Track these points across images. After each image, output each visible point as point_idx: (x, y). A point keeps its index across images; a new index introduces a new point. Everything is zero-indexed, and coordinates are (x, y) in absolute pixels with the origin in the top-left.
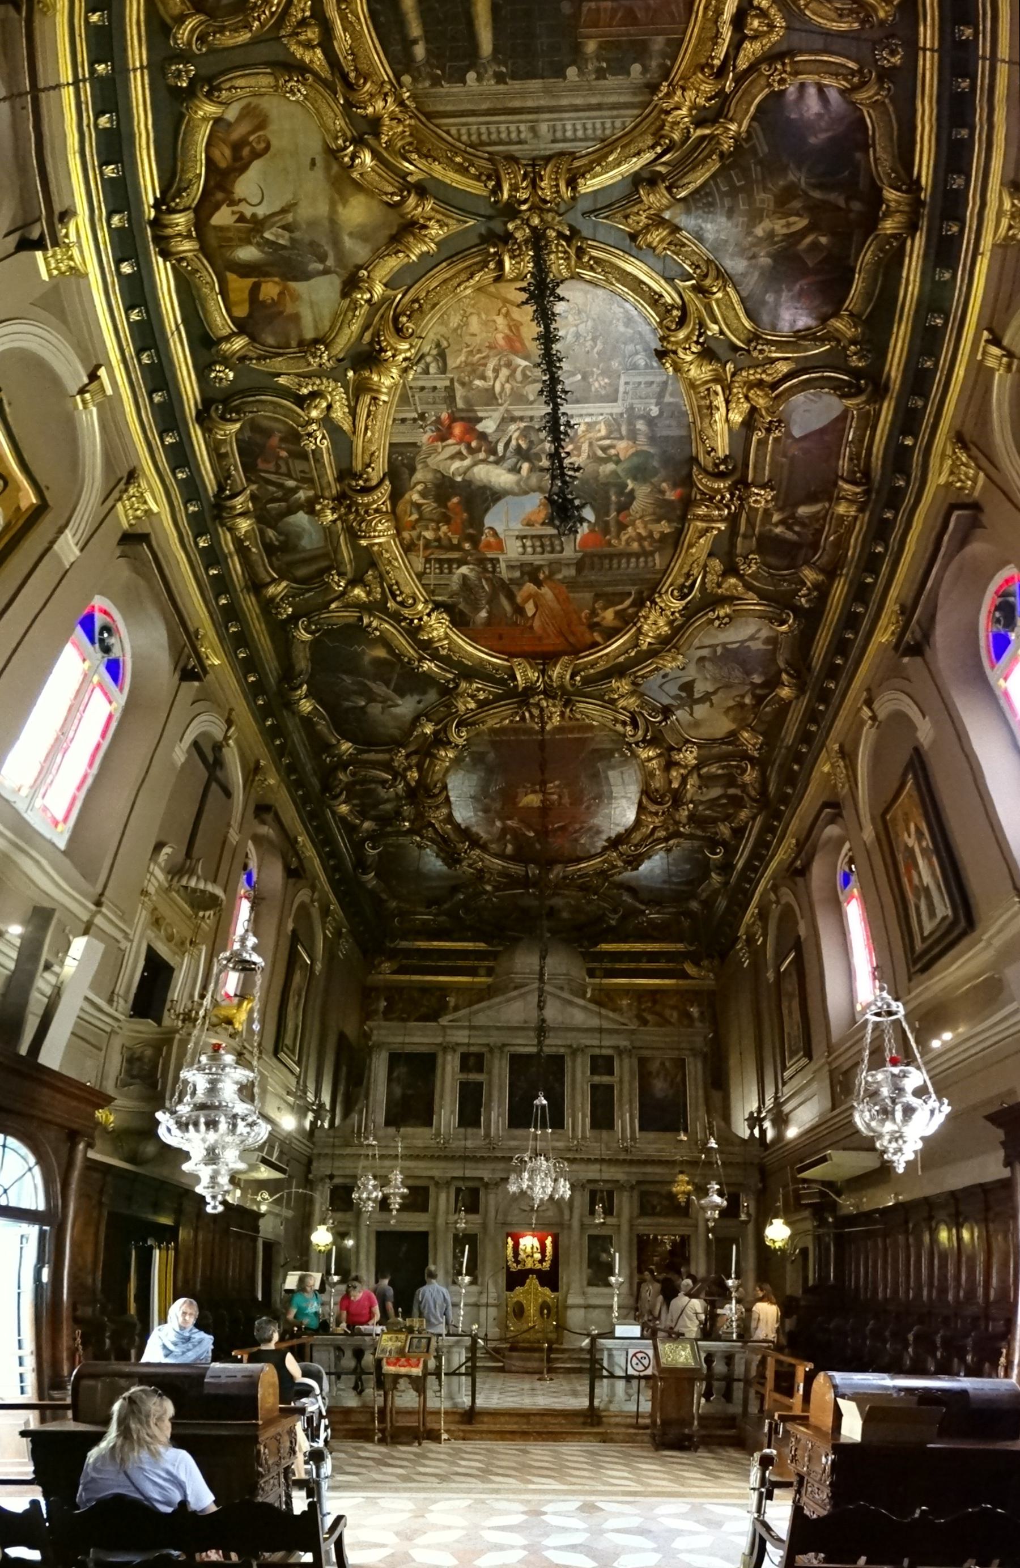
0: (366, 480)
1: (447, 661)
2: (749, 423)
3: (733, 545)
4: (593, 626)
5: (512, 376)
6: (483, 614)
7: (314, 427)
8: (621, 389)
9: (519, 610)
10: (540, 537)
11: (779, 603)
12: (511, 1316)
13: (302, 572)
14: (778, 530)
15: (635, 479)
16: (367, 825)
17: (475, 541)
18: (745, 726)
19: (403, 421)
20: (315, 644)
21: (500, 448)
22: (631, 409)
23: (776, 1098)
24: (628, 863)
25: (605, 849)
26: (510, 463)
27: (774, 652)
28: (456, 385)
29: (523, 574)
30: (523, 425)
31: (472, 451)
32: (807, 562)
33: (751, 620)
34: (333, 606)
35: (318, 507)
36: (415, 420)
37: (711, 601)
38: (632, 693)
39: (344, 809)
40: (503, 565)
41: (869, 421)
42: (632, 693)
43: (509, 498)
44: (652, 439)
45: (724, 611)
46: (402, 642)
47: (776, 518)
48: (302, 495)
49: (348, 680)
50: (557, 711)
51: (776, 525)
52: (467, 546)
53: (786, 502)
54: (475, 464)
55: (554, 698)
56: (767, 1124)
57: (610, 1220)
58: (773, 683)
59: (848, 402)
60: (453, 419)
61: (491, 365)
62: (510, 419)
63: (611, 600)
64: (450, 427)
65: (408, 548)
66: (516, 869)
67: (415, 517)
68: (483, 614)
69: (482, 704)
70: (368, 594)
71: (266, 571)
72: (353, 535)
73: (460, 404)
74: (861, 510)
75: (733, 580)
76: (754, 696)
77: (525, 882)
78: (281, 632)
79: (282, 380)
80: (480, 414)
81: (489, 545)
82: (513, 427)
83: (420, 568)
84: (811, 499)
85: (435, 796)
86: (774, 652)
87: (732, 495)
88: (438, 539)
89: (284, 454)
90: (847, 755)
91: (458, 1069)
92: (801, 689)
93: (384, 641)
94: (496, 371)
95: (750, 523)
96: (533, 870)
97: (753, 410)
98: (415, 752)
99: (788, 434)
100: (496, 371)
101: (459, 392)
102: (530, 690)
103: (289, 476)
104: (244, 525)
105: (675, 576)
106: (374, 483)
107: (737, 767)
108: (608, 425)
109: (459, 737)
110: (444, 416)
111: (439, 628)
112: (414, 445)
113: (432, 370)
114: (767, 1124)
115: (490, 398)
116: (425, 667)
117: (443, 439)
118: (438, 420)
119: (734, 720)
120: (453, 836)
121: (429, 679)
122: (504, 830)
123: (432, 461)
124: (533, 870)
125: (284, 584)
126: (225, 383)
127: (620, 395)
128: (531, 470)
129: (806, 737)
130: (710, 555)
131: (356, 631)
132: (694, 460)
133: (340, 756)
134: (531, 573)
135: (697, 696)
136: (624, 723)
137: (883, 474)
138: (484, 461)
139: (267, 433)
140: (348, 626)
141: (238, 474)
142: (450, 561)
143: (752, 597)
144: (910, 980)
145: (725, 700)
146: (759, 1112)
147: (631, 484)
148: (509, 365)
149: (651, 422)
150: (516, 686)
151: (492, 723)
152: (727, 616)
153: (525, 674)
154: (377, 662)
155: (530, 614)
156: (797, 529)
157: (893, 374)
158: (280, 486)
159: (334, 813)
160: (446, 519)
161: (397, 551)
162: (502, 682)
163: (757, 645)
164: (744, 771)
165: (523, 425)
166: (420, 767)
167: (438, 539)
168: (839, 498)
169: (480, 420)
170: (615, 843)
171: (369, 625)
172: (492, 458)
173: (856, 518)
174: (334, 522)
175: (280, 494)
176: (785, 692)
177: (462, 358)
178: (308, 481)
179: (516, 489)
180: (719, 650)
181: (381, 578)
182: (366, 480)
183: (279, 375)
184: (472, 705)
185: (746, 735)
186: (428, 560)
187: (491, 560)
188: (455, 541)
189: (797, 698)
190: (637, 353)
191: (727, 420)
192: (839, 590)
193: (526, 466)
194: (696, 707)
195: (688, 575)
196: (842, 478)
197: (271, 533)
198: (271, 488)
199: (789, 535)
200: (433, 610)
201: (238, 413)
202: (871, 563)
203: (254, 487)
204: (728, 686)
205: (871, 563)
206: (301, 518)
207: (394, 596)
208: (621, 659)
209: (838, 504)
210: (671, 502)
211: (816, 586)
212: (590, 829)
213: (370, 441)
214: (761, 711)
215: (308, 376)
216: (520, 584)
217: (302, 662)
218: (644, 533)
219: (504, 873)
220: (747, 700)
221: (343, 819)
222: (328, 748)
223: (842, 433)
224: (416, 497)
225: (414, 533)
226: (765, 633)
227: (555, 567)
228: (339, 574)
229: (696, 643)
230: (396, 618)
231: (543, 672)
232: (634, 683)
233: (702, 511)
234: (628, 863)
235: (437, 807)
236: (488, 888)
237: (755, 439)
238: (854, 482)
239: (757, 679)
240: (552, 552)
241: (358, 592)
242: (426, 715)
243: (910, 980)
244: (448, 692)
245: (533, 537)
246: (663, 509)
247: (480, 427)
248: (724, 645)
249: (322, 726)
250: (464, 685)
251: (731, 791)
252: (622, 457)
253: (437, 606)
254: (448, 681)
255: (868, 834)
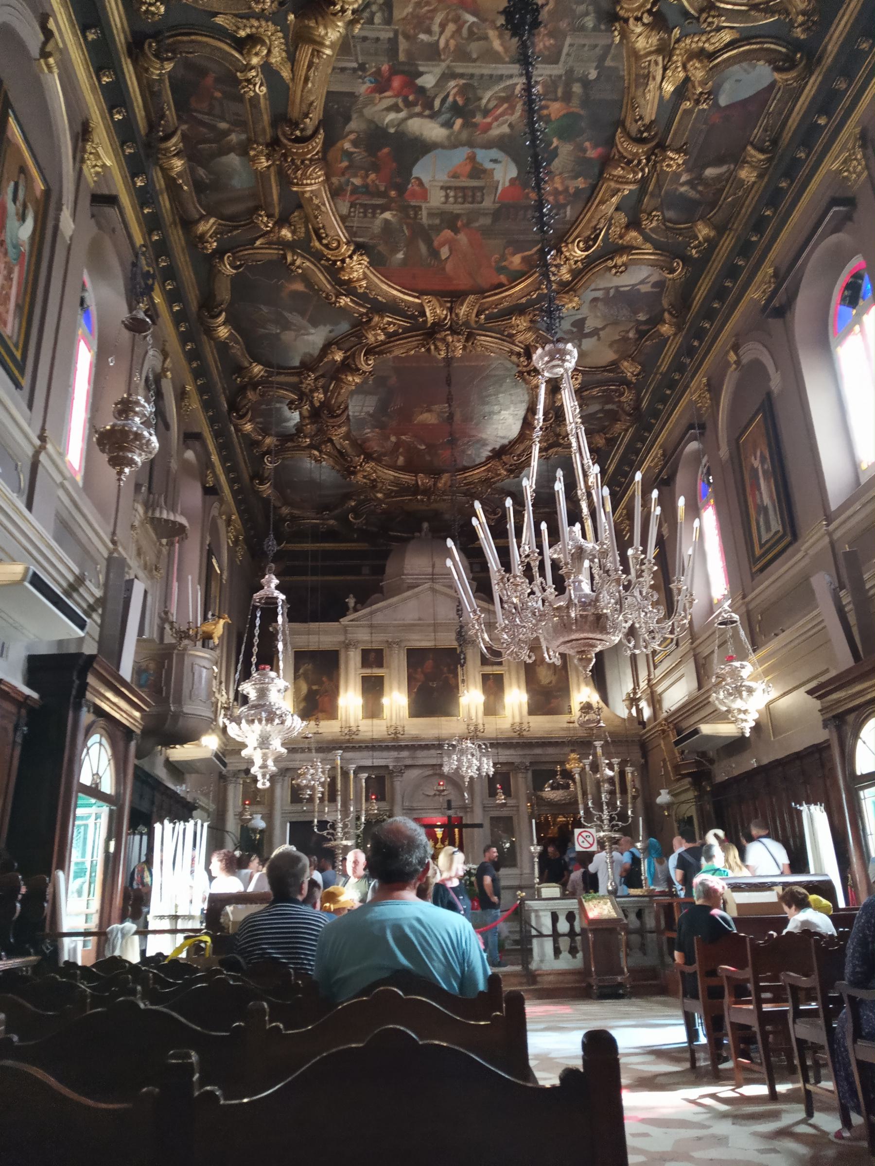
0: (302, 130)
1: (363, 298)
2: (682, 91)
3: (640, 201)
4: (501, 270)
5: (458, 31)
6: (400, 255)
7: (253, 73)
8: (565, 50)
9: (434, 253)
10: (463, 189)
11: (670, 252)
12: (576, 912)
13: (231, 210)
14: (683, 189)
15: (560, 138)
16: (268, 440)
17: (401, 189)
18: (625, 356)
19: (343, 70)
20: (235, 280)
21: (437, 103)
22: (570, 72)
23: (649, 680)
24: (511, 471)
25: (489, 458)
26: (445, 117)
27: (659, 295)
28: (401, 39)
29: (442, 221)
30: (462, 82)
31: (409, 104)
32: (702, 218)
33: (643, 267)
34: (258, 243)
35: (252, 153)
36: (354, 70)
37: (612, 250)
38: (529, 329)
39: (248, 427)
40: (424, 213)
41: (794, 95)
42: (529, 329)
43: (438, 151)
44: (586, 102)
45: (619, 260)
46: (322, 279)
47: (684, 178)
48: (233, 138)
49: (265, 309)
50: (460, 345)
51: (683, 184)
52: (393, 193)
53: (696, 166)
54: (411, 116)
55: (459, 334)
56: (643, 704)
57: (511, 802)
58: (656, 320)
59: (777, 76)
60: (394, 72)
61: (438, 19)
62: (445, 77)
63: (519, 247)
64: (389, 80)
65: (335, 193)
66: (406, 478)
67: (345, 164)
68: (400, 255)
69: (389, 335)
70: (293, 233)
71: (195, 209)
72: (285, 181)
73: (402, 57)
74: (760, 176)
75: (634, 234)
76: (638, 332)
77: (415, 490)
78: (207, 266)
79: (219, 20)
80: (421, 69)
81: (414, 195)
82: (452, 84)
83: (345, 211)
84: (719, 161)
85: (339, 416)
86: (659, 295)
87: (648, 160)
88: (366, 186)
89: (218, 94)
90: (713, 388)
91: (359, 664)
92: (679, 328)
93: (305, 278)
94: (443, 26)
95: (659, 186)
96: (423, 480)
97: (687, 79)
98: (322, 376)
99: (716, 104)
100: (443, 26)
101: (403, 45)
102: (438, 325)
103: (223, 119)
104: (178, 164)
105: (583, 229)
106: (309, 132)
107: (615, 391)
108: (545, 85)
109: (367, 365)
110: (385, 67)
111: (358, 268)
112: (352, 95)
113: (378, 19)
114: (643, 704)
115: (433, 53)
116: (342, 302)
117: (382, 91)
118: (378, 71)
119: (616, 352)
120: (349, 450)
121: (344, 311)
122: (397, 445)
123: (368, 112)
124: (423, 480)
125: (212, 220)
126: (157, 18)
127: (563, 57)
128: (463, 126)
129: (680, 368)
130: (617, 209)
131: (281, 267)
132: (621, 123)
133: (251, 378)
134: (451, 221)
135: (587, 331)
136: (519, 355)
137: (788, 144)
138: (419, 115)
139: (202, 72)
140: (270, 262)
141: (170, 113)
142: (375, 207)
143: (648, 248)
144: (753, 579)
145: (612, 334)
146: (635, 693)
147: (555, 142)
148: (457, 20)
149: (586, 83)
150: (425, 322)
151: (398, 352)
152: (624, 264)
153: (434, 311)
154: (295, 294)
155: (444, 257)
156: (700, 188)
157: (830, 47)
158: (213, 128)
159: (238, 430)
160: (375, 167)
161: (325, 196)
162: (413, 317)
163: (645, 288)
164: (622, 394)
165: (462, 82)
166: (326, 390)
167: (366, 186)
168: (745, 162)
169: (421, 74)
170: (499, 453)
171: (294, 261)
172: (427, 112)
173: (754, 183)
174: (268, 167)
175: (211, 135)
176: (666, 329)
177: (410, 9)
178: (240, 124)
179: (446, 143)
180: (612, 292)
181: (307, 220)
182: (302, 130)
183: (216, 14)
184: (382, 337)
185: (626, 364)
186: (353, 205)
187: (415, 207)
188: (383, 189)
189: (675, 335)
190: (587, 14)
191: (660, 88)
192: (727, 243)
193: (459, 122)
194: (584, 341)
195: (595, 228)
196: (752, 144)
197: (201, 172)
198: (203, 130)
199: (692, 194)
200: (354, 252)
201: (174, 52)
202: (759, 225)
203: (184, 127)
204: (615, 323)
205: (759, 225)
206: (233, 160)
207: (320, 239)
208: (524, 300)
209: (742, 168)
210: (590, 160)
211: (707, 239)
212: (478, 441)
213: (310, 91)
214: (642, 342)
215: (247, 17)
216: (438, 229)
217: (224, 293)
218: (560, 188)
219: (396, 482)
220: (631, 335)
221: (246, 436)
222: (240, 370)
223: (764, 103)
224: (347, 146)
225: (343, 179)
226: (655, 278)
227: (472, 217)
228: (268, 216)
229: (593, 286)
230: (318, 257)
231: (451, 310)
232: (531, 321)
233: (619, 172)
234: (511, 471)
235: (339, 426)
236: (380, 495)
237: (683, 107)
238: (761, 150)
239: (642, 317)
240: (472, 203)
241: (286, 233)
242: (336, 343)
243: (753, 579)
244: (360, 326)
245: (456, 188)
246: (581, 166)
247: (420, 81)
248: (617, 288)
249: (237, 349)
250: (376, 319)
251: (609, 407)
252: (553, 117)
253: (360, 248)
254: (362, 315)
255: (724, 452)
